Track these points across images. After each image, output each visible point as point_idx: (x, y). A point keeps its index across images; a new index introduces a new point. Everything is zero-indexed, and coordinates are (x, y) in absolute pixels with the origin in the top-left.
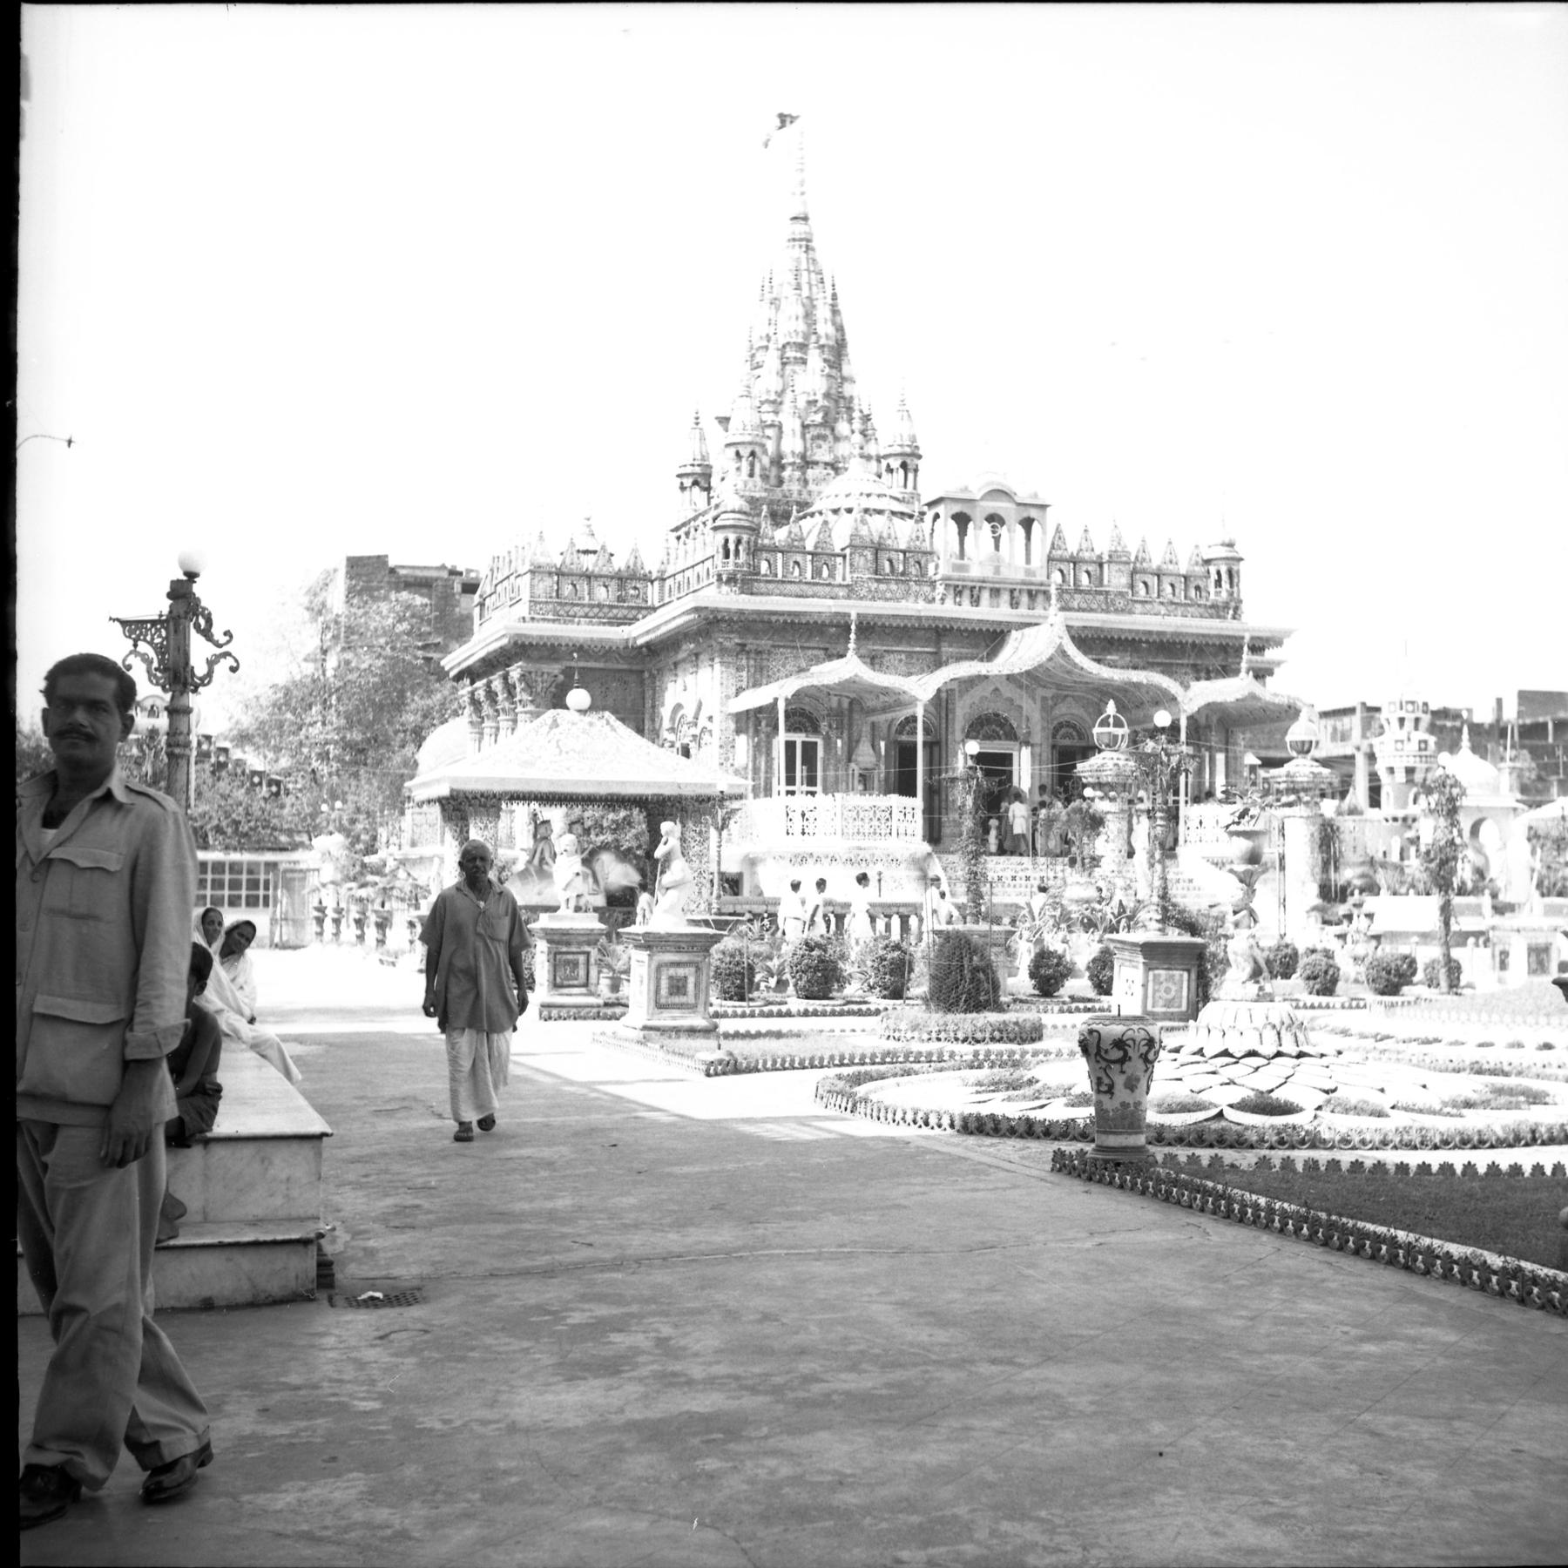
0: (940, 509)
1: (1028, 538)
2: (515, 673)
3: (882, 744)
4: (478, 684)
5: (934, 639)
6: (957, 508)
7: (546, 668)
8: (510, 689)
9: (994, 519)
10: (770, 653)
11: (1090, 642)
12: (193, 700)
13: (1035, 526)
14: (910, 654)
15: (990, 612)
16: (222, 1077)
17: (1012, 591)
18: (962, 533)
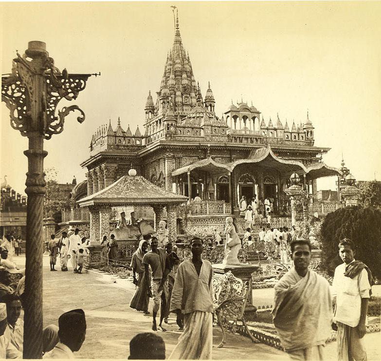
0: (229, 114)
1: (254, 123)
2: (103, 165)
3: (215, 185)
4: (91, 170)
5: (229, 152)
6: (234, 114)
7: (112, 165)
8: (101, 171)
9: (245, 118)
10: (182, 158)
11: (277, 152)
12: (47, 145)
13: (256, 119)
14: (222, 158)
15: (245, 144)
16: (26, 177)
17: (251, 138)
18: (235, 121)
